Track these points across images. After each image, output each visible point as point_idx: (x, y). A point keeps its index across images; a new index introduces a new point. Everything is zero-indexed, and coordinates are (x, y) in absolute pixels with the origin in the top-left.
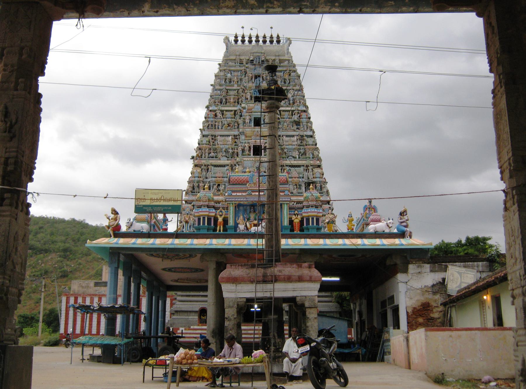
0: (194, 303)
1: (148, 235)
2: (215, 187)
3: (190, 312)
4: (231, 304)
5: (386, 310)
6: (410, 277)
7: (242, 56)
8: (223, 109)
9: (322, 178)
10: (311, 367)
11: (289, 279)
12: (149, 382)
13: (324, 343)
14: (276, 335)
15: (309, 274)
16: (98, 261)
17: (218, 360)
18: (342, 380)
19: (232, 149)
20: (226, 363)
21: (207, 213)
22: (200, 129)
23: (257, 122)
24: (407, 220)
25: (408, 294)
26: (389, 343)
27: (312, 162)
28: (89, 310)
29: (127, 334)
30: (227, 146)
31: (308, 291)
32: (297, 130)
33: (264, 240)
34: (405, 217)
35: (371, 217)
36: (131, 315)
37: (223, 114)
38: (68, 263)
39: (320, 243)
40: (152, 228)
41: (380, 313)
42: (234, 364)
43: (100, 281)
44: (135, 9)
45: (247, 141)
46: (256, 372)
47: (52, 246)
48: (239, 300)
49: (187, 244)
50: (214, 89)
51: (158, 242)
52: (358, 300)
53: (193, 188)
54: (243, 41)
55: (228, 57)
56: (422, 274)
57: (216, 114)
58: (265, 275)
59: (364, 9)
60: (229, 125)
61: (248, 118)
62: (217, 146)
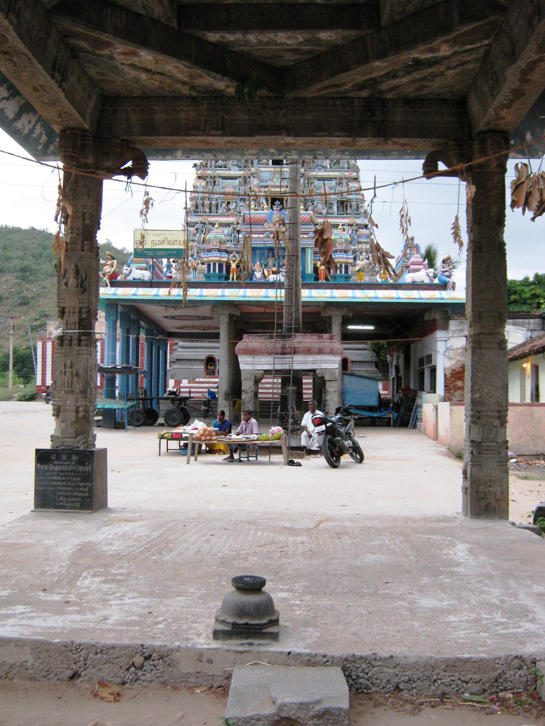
0: (199, 350)
1: (150, 284)
2: (224, 205)
3: (195, 360)
4: (248, 376)
5: (424, 369)
6: (451, 334)
11: (308, 351)
12: (165, 455)
14: (295, 407)
18: (358, 457)
20: (244, 439)
21: (218, 259)
27: (346, 174)
35: (412, 260)
38: (29, 286)
39: (348, 295)
44: (169, 155)
47: (6, 264)
48: (256, 372)
51: (162, 293)
53: (197, 207)
59: (372, 157)
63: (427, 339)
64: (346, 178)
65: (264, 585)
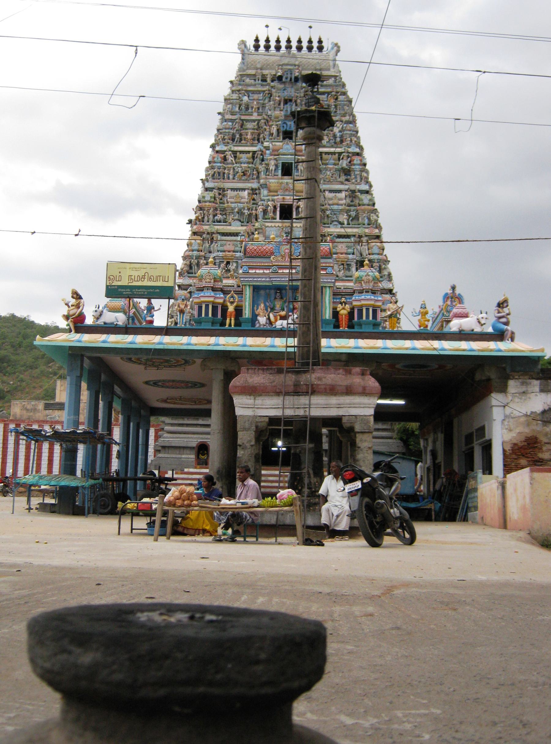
0: (190, 436)
1: (125, 330)
2: (223, 265)
3: (184, 448)
4: (247, 425)
5: (473, 448)
7: (266, 69)
8: (236, 149)
9: (382, 254)
10: (362, 512)
11: (332, 391)
13: (381, 481)
14: (311, 472)
15: (362, 384)
16: (48, 377)
17: (228, 502)
18: (407, 536)
19: (249, 209)
20: (239, 505)
21: (212, 299)
22: (202, 180)
23: (287, 170)
24: (508, 314)
25: (506, 423)
26: (476, 494)
27: (367, 231)
28: (38, 438)
29: (92, 474)
30: (241, 205)
31: (360, 407)
32: (346, 182)
33: (296, 339)
34: (505, 309)
35: (455, 310)
36: (99, 446)
37: (235, 157)
39: (377, 345)
40: (130, 321)
41: (464, 452)
42: (250, 507)
43: (52, 402)
45: (270, 198)
46: (281, 524)
49: (182, 344)
50: (224, 120)
51: (141, 341)
52: (432, 435)
54: (267, 47)
55: (244, 71)
56: (528, 395)
57: (225, 157)
58: (297, 385)
60: (244, 174)
61: (273, 163)
62: (226, 205)
63: (477, 409)
64: (366, 236)
65: (315, 674)
